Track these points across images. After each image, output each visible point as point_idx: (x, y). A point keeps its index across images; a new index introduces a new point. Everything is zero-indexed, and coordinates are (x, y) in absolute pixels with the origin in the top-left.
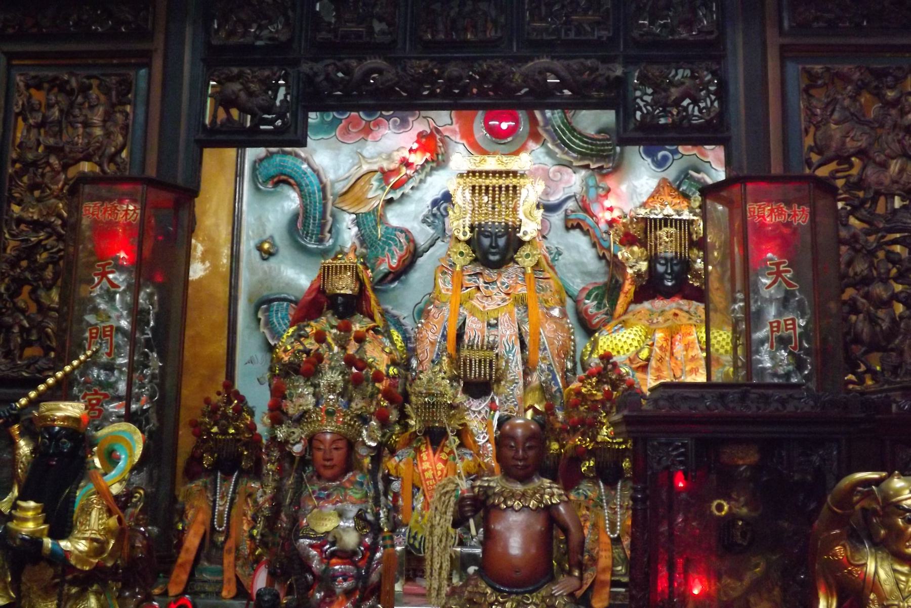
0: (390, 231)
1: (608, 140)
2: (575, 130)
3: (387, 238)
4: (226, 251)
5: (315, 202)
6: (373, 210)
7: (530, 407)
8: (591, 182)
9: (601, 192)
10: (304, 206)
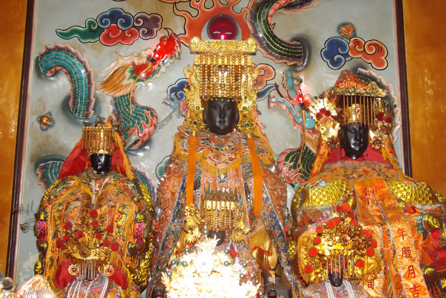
0: (139, 109)
1: (299, 46)
2: (276, 37)
3: (137, 114)
4: (14, 123)
5: (82, 86)
6: (127, 95)
7: (255, 248)
8: (289, 75)
9: (295, 82)
10: (74, 91)
